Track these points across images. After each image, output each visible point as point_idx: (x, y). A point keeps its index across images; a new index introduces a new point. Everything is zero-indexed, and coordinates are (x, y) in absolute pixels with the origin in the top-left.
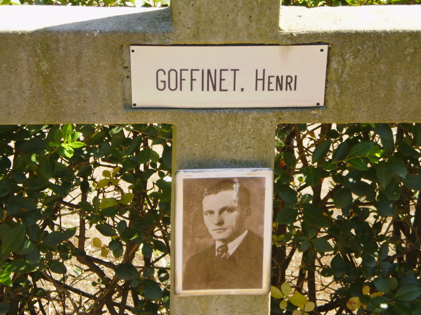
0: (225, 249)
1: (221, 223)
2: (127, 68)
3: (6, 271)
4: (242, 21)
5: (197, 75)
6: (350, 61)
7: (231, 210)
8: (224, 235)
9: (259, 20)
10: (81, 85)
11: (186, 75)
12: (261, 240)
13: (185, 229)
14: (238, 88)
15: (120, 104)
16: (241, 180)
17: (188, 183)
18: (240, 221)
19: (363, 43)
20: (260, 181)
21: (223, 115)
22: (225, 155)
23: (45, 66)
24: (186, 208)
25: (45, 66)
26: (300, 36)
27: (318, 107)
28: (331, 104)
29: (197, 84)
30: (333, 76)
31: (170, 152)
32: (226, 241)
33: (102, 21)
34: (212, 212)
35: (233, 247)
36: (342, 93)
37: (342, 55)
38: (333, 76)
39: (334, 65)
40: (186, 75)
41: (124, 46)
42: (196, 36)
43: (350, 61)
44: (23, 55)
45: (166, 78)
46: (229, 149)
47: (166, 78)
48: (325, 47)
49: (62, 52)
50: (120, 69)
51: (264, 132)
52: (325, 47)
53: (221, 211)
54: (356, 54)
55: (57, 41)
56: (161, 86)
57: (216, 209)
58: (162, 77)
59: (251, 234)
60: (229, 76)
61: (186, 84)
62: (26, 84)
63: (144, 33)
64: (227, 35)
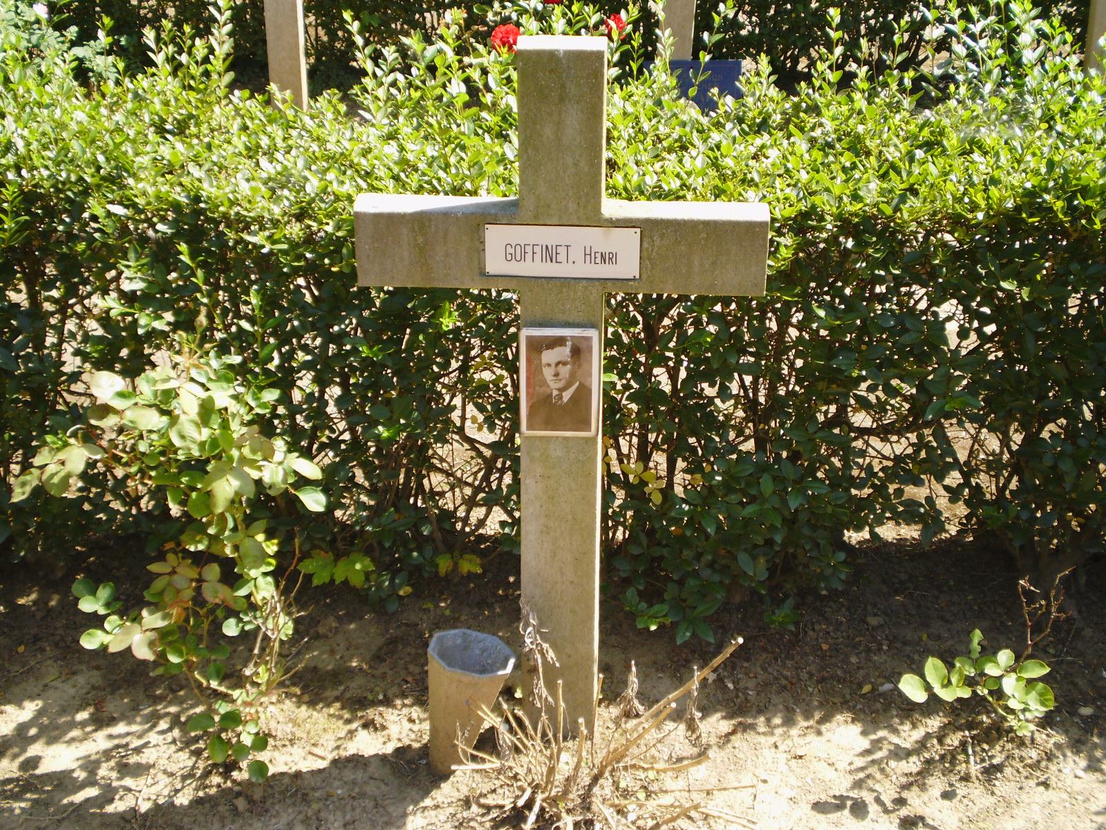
0: (561, 397)
1: (557, 375)
2: (483, 243)
3: (159, 575)
4: (572, 207)
5: (538, 249)
6: (657, 242)
7: (565, 364)
8: (561, 385)
9: (585, 207)
10: (447, 255)
11: (529, 249)
12: (590, 391)
13: (528, 378)
14: (570, 260)
15: (476, 271)
16: (572, 337)
17: (530, 340)
18: (573, 376)
19: (667, 228)
20: (589, 339)
21: (558, 283)
22: (561, 317)
23: (420, 240)
24: (529, 360)
25: (420, 240)
26: (618, 220)
27: (634, 279)
28: (644, 276)
29: (538, 256)
30: (645, 254)
31: (69, 708)
32: (561, 390)
33: (466, 206)
34: (549, 365)
35: (567, 395)
36: (652, 268)
37: (651, 237)
38: (645, 254)
39: (645, 245)
40: (529, 249)
41: (1050, 795)
42: (536, 217)
43: (657, 242)
44: (405, 231)
45: (512, 251)
46: (563, 312)
47: (512, 251)
48: (638, 230)
49: (433, 229)
50: (477, 243)
51: (592, 298)
52: (638, 230)
53: (557, 364)
54: (662, 236)
55: (430, 220)
56: (509, 257)
57: (553, 362)
58: (510, 250)
59: (581, 385)
60: (562, 250)
61: (529, 256)
62: (406, 254)
63: (496, 215)
64: (560, 218)
